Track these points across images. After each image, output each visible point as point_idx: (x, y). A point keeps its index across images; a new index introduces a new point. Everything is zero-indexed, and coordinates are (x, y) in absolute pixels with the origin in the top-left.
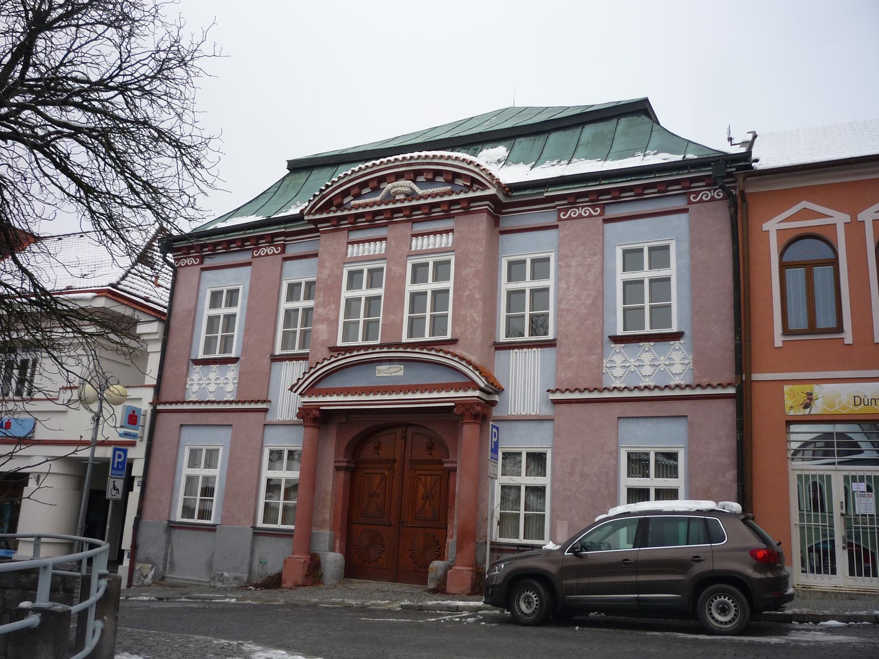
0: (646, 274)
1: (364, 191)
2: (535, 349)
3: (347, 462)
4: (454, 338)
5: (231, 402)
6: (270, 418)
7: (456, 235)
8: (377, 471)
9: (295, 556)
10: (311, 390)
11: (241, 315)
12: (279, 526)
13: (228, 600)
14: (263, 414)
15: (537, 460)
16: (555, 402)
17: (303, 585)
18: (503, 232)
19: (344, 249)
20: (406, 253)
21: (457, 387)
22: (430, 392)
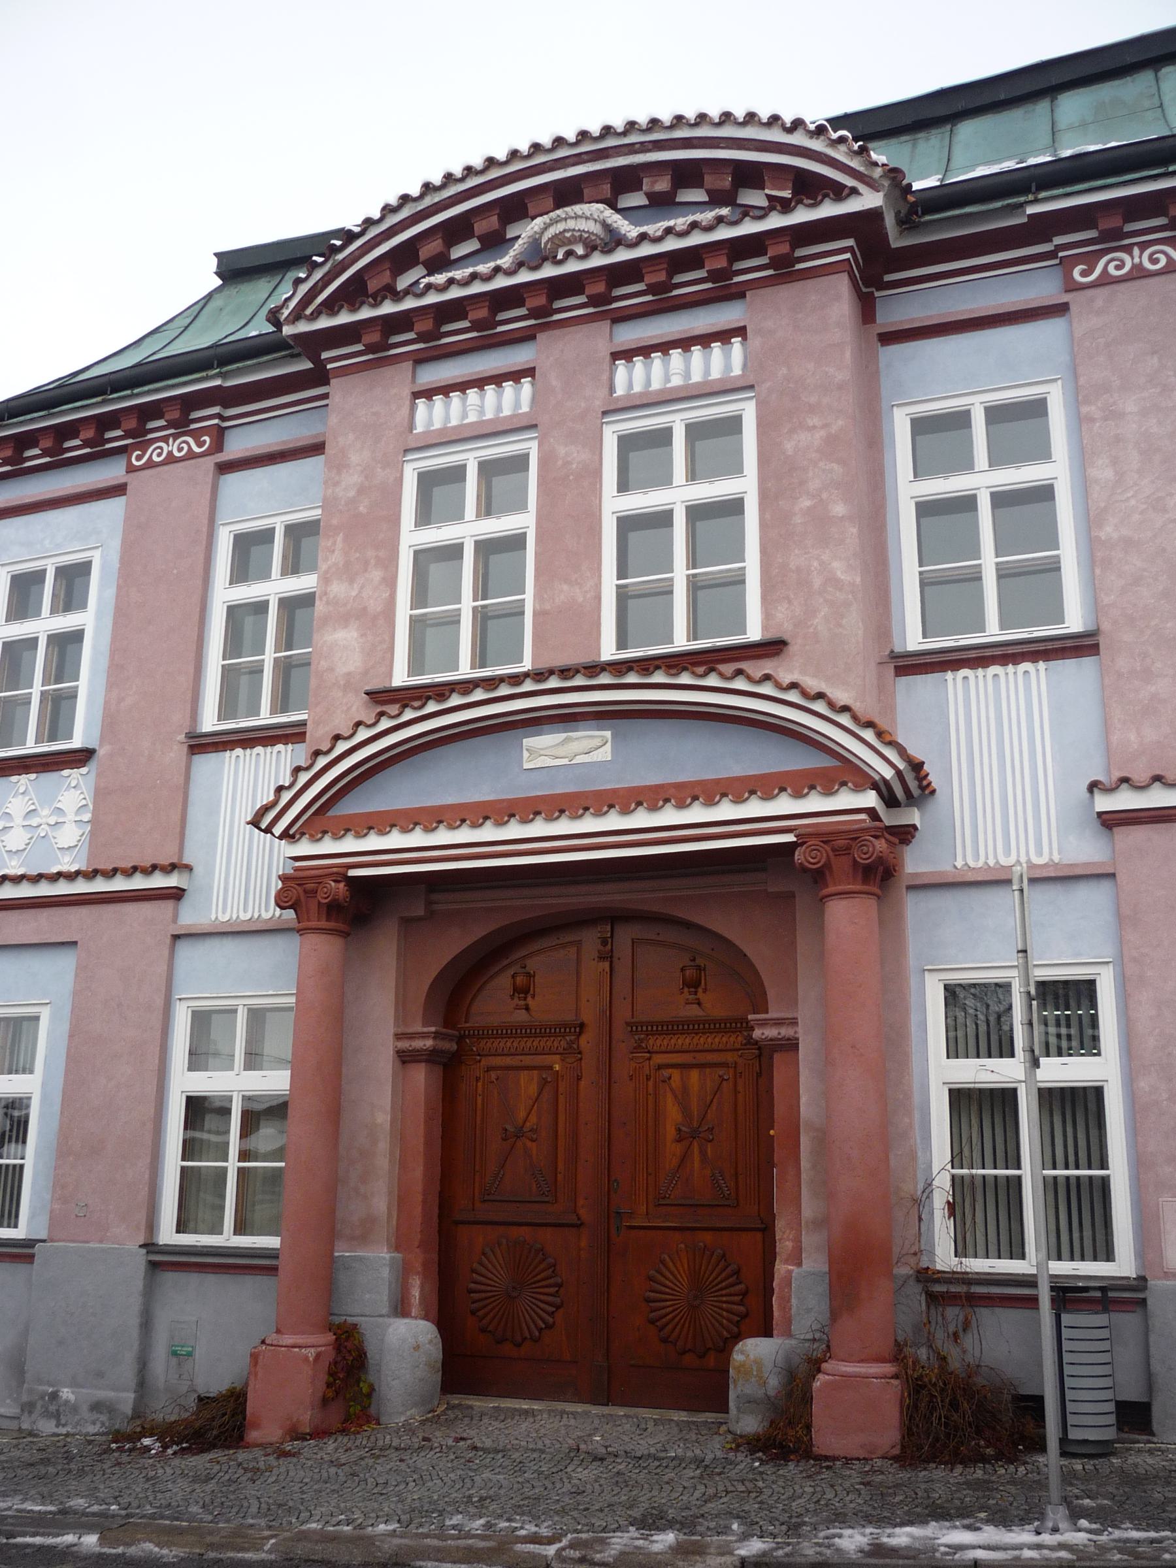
0: (983, 480)
1: (457, 252)
2: (1026, 666)
3: (436, 1036)
4: (771, 635)
5: (71, 877)
6: (189, 916)
7: (755, 341)
8: (528, 1060)
9: (288, 1340)
10: (320, 819)
11: (97, 630)
12: (228, 1238)
13: (69, 1538)
14: (169, 905)
15: (1068, 1007)
16: (1110, 821)
17: (319, 1433)
18: (890, 338)
19: (405, 410)
20: (599, 405)
21: (799, 784)
22: (710, 802)
